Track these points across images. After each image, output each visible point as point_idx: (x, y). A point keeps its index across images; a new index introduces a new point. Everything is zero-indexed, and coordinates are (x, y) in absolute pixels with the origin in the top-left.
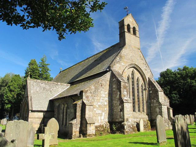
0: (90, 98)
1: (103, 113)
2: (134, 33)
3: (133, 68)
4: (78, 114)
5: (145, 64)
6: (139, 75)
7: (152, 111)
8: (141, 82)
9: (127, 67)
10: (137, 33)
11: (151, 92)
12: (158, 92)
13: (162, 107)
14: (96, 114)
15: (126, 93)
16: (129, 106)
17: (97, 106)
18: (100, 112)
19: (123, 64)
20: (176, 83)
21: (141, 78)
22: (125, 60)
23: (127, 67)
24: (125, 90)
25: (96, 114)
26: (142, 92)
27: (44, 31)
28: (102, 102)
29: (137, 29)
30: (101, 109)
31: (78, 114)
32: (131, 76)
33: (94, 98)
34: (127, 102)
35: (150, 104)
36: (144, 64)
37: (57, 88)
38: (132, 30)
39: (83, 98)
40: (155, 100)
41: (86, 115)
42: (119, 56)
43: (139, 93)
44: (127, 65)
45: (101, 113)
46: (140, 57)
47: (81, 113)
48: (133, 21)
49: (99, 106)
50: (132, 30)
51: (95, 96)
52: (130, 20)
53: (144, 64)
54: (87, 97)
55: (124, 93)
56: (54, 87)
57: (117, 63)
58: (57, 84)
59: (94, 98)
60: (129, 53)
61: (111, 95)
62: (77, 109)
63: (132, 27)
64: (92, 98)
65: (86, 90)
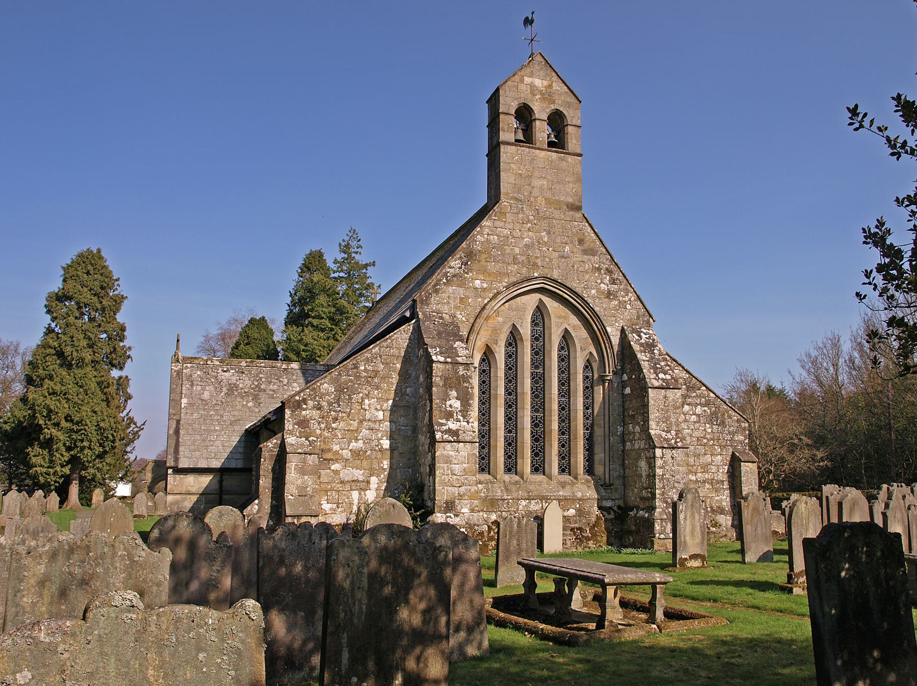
0: (314, 425)
1: (374, 480)
2: (558, 143)
3: (537, 296)
4: (265, 482)
5: (609, 272)
6: (573, 320)
7: (627, 470)
8: (583, 348)
9: (498, 293)
10: (573, 140)
11: (628, 390)
12: (647, 392)
13: (654, 457)
14: (342, 482)
15: (457, 404)
16: (464, 453)
17: (346, 454)
18: (359, 474)
19: (478, 283)
20: (317, 401)
21: (580, 335)
22: (492, 267)
23: (498, 293)
24: (454, 393)
25: (342, 482)
26: (589, 390)
27: (848, 108)
28: (367, 441)
29: (572, 116)
30: (365, 463)
31: (265, 482)
32: (526, 331)
33: (334, 425)
34: (450, 438)
35: (624, 442)
36: (599, 269)
37: (286, 381)
38: (542, 132)
39: (284, 429)
40: (638, 424)
41: (287, 486)
42: (459, 253)
43: (569, 398)
44: (501, 286)
45: (361, 478)
46: (581, 242)
47: (274, 479)
48: (550, 86)
49: (357, 454)
50: (542, 132)
51: (336, 419)
52: (532, 86)
53: (599, 269)
54: (303, 423)
55: (448, 403)
56: (270, 382)
57: (448, 283)
58: (284, 366)
59: (334, 425)
60: (517, 233)
61: (415, 412)
62: (262, 467)
63: (541, 111)
64: (323, 426)
65: (297, 398)
